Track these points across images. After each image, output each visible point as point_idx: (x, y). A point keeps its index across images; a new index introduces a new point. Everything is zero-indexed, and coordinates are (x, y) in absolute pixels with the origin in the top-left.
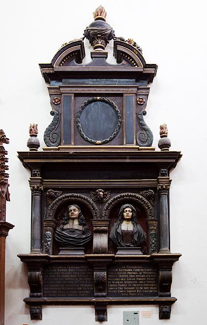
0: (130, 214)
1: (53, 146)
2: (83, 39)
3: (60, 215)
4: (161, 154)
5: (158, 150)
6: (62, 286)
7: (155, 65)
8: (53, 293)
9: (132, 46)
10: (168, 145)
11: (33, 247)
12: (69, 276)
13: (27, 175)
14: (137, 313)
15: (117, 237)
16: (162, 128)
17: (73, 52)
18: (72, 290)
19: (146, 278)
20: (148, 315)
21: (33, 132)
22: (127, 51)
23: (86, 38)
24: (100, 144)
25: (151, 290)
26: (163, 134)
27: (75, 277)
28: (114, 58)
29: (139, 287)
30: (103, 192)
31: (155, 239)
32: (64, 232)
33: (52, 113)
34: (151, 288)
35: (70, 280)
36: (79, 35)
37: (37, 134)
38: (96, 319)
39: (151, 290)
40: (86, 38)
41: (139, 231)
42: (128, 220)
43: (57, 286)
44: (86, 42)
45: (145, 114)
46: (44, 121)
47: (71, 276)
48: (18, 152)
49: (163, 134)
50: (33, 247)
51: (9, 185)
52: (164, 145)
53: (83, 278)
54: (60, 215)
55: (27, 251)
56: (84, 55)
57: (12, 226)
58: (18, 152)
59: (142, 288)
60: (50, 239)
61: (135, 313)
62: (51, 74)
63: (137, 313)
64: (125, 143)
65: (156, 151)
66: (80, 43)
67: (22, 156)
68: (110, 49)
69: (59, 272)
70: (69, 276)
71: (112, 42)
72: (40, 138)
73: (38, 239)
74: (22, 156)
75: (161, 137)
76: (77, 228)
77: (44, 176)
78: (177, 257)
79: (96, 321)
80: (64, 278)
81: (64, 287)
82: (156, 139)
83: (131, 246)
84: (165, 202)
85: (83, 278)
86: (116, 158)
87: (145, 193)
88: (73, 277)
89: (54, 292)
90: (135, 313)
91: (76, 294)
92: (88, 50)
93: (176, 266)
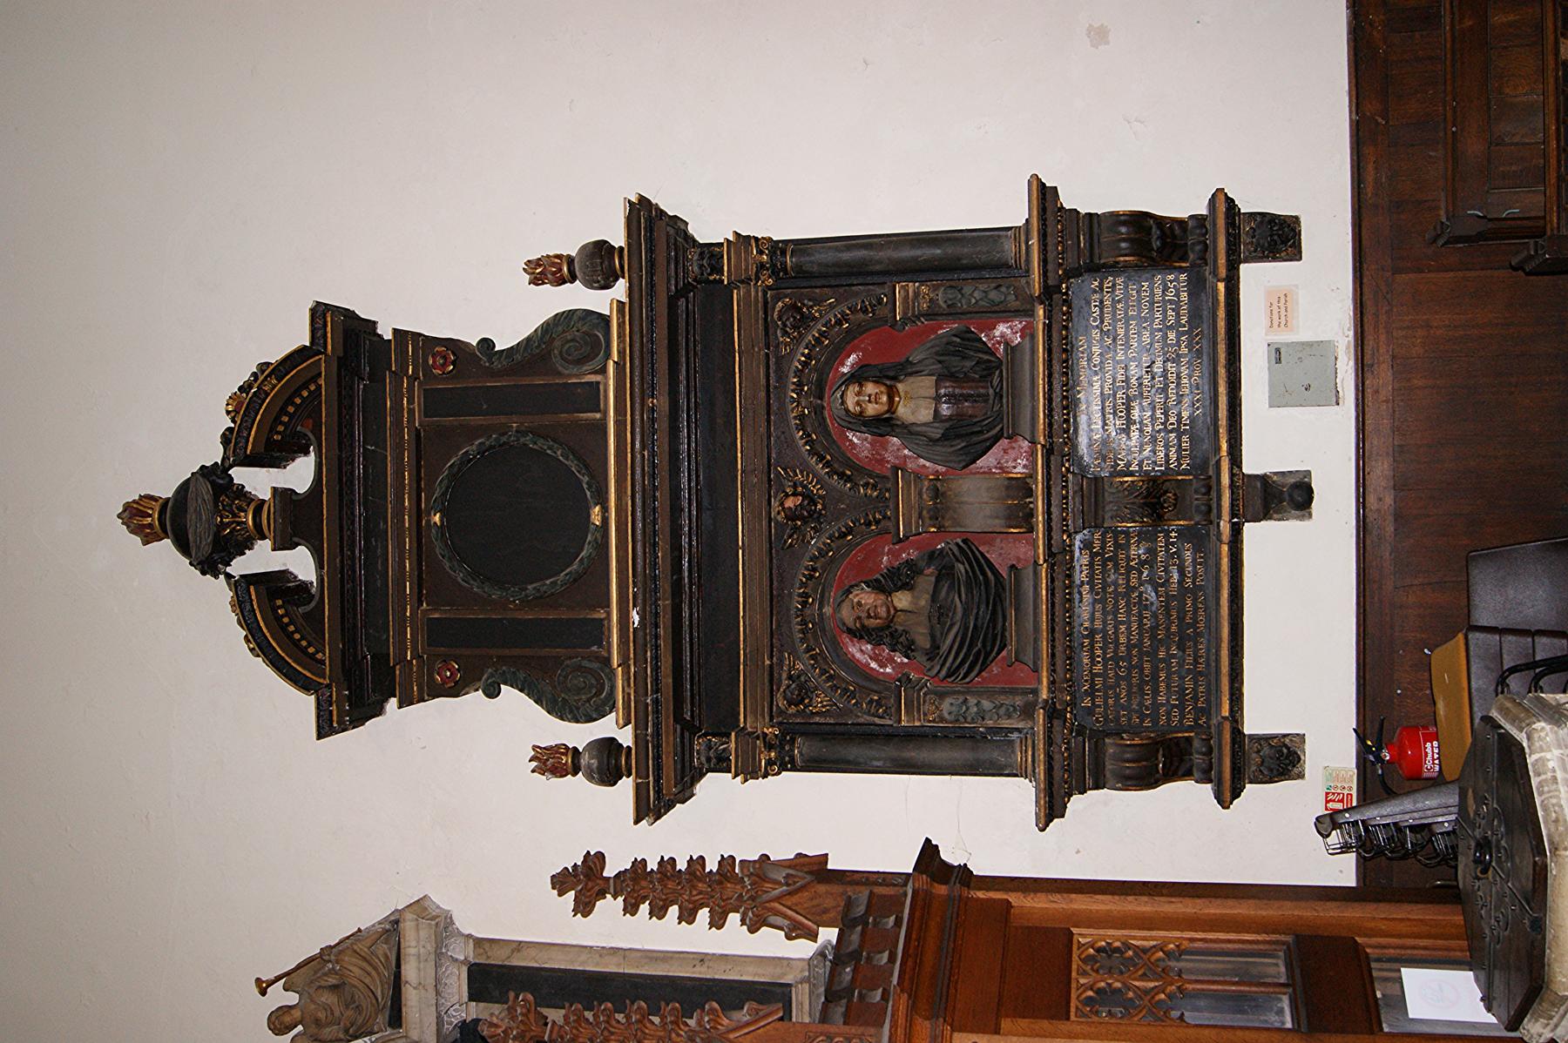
0: (870, 388)
1: (613, 688)
2: (229, 576)
3: (873, 665)
4: (636, 281)
5: (620, 290)
6: (1162, 655)
7: (313, 311)
8: (1195, 690)
9: (246, 403)
10: (600, 249)
11: (1006, 766)
12: (1123, 628)
13: (715, 787)
14: (1278, 351)
15: (958, 436)
16: (536, 280)
17: (273, 620)
18: (1181, 619)
19: (1127, 319)
20: (1281, 307)
21: (553, 762)
22: (271, 412)
23: (228, 569)
24: (605, 510)
25: (1177, 295)
26: (546, 271)
27: (1128, 604)
28: (292, 466)
29: (1165, 345)
30: (787, 495)
31: (967, 290)
32: (945, 647)
33: (493, 693)
34: (1170, 296)
35: (1141, 625)
36: (218, 591)
37: (567, 747)
38: (1301, 518)
39: (1177, 295)
40: (228, 569)
41: (937, 353)
42: (936, 411)
43: (1163, 675)
44: (242, 566)
45: (487, 344)
46: (513, 720)
47: (1121, 617)
48: (636, 822)
49: (546, 271)
50: (1006, 766)
51: (765, 857)
52: (598, 263)
53: (1129, 569)
54: (873, 665)
55: (1020, 794)
56: (284, 575)
57: (929, 851)
58: (636, 822)
59: (1172, 336)
60: (972, 701)
61: (1279, 361)
62: (349, 700)
63: (1278, 351)
64: (598, 416)
65: (624, 299)
66: (243, 586)
67: (650, 807)
68: (258, 481)
69: (1105, 665)
70: (1123, 628)
71: (240, 475)
72: (579, 735)
73: (973, 752)
74: (650, 807)
75: (573, 279)
76: (927, 596)
77: (725, 724)
78: (1044, 196)
79: (1310, 515)
80: (1129, 647)
81: (1168, 649)
82: (578, 297)
83: (995, 383)
84: (1381, 470)
85: (1129, 569)
86: (1218, 661)
87: (785, 333)
88: (1128, 613)
89: (1189, 685)
90: (1279, 361)
91: (1195, 600)
92: (261, 558)
93: (1078, 198)
